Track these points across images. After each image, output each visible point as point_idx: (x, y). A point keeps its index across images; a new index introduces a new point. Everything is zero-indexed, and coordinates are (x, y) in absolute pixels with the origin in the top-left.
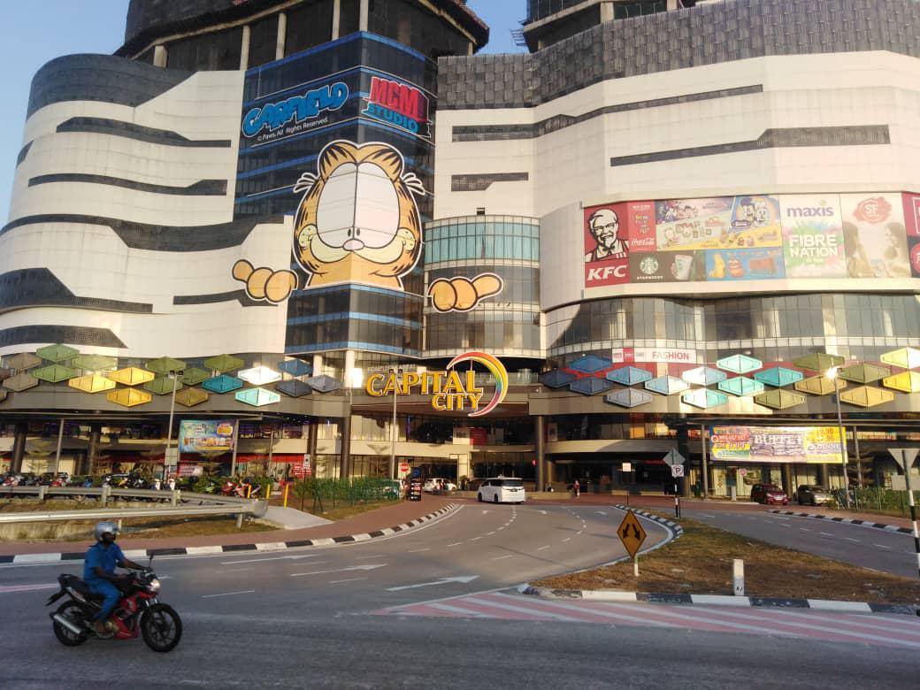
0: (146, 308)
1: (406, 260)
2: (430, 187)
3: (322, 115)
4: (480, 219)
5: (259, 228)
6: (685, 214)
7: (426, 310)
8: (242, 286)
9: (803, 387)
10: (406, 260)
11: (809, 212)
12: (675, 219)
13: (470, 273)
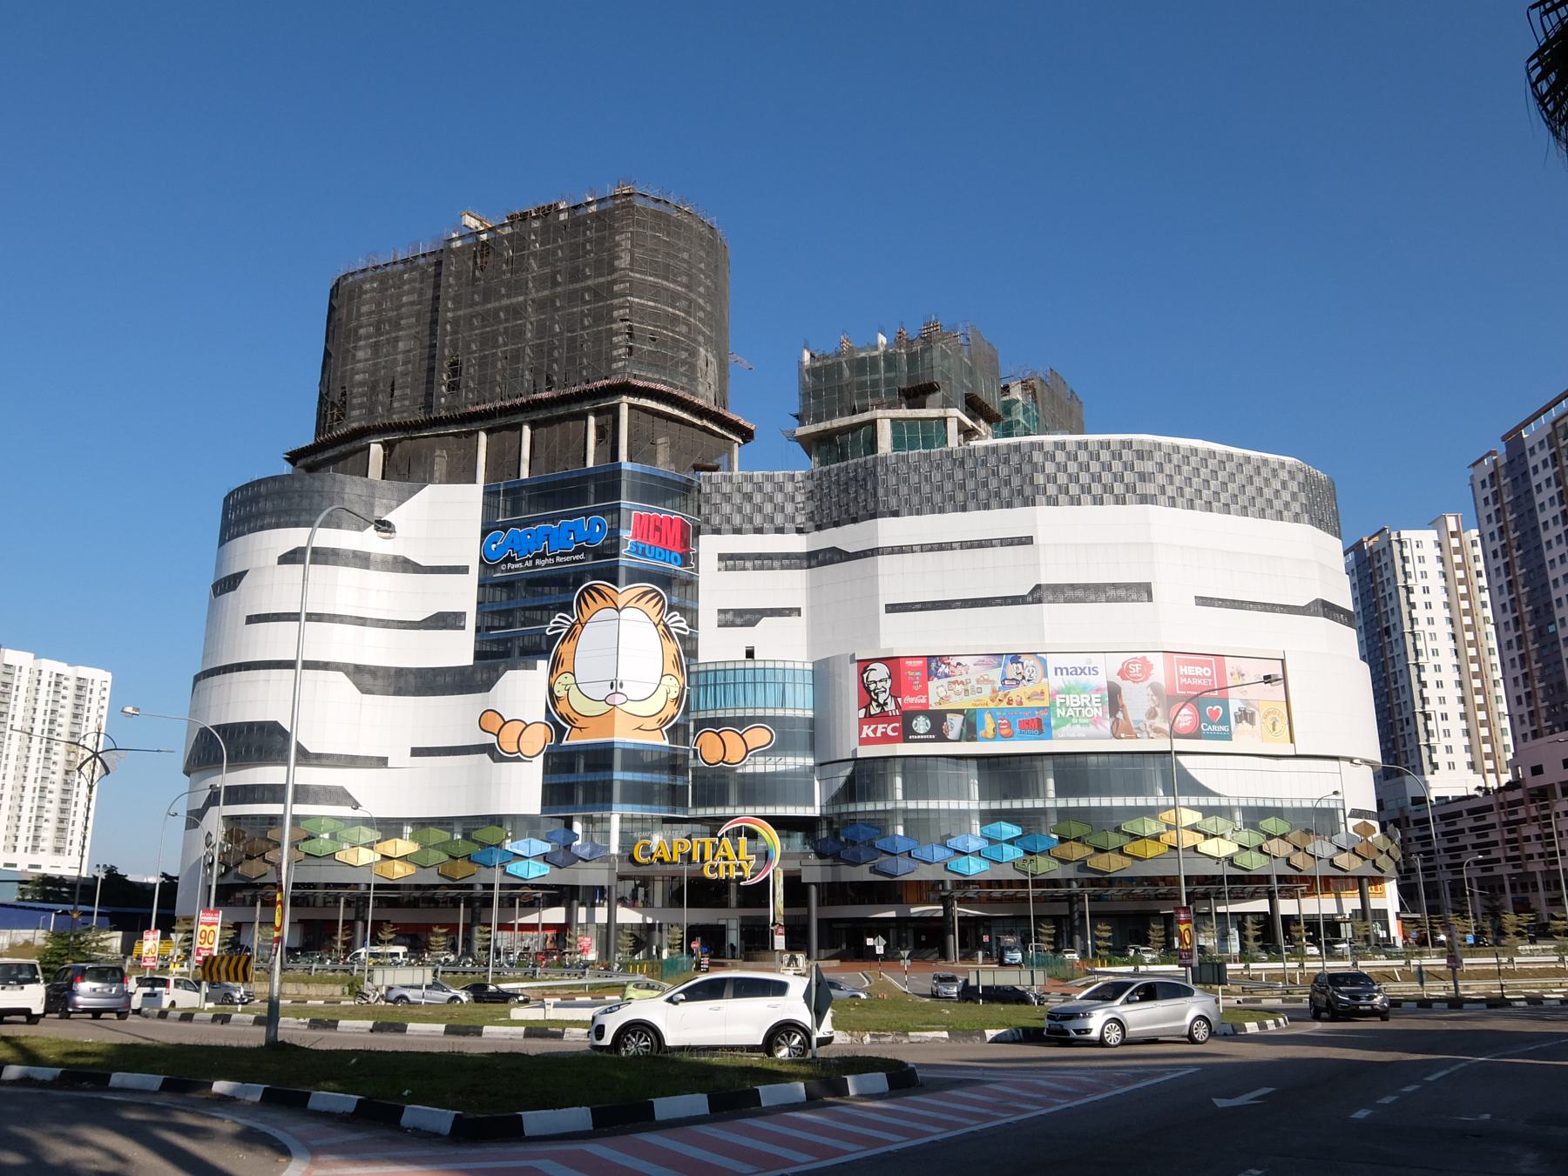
0: (382, 762)
1: (671, 709)
2: (693, 625)
3: (578, 551)
4: (750, 665)
5: (510, 675)
6: (957, 671)
7: (692, 763)
8: (492, 739)
9: (1057, 853)
10: (671, 709)
11: (1076, 671)
12: (947, 676)
13: (741, 723)
